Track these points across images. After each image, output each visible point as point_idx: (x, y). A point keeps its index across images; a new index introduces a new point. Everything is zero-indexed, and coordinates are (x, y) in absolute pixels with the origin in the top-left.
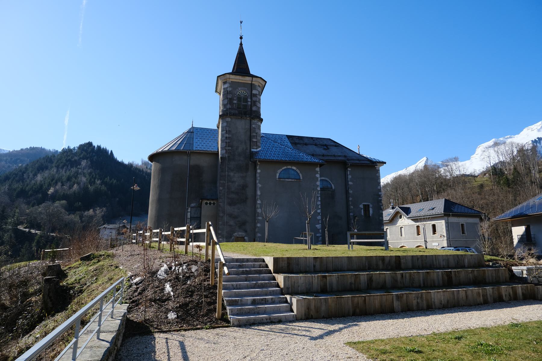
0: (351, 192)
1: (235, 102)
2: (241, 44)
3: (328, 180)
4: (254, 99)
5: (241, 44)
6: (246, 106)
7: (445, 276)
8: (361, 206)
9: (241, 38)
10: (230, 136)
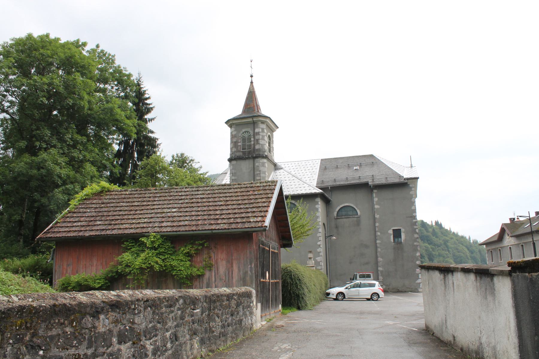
0: (377, 216)
1: (240, 144)
2: (252, 83)
3: (352, 205)
4: (257, 137)
5: (252, 83)
6: (250, 146)
7: (303, 305)
8: (391, 232)
9: (252, 76)
10: (236, 178)
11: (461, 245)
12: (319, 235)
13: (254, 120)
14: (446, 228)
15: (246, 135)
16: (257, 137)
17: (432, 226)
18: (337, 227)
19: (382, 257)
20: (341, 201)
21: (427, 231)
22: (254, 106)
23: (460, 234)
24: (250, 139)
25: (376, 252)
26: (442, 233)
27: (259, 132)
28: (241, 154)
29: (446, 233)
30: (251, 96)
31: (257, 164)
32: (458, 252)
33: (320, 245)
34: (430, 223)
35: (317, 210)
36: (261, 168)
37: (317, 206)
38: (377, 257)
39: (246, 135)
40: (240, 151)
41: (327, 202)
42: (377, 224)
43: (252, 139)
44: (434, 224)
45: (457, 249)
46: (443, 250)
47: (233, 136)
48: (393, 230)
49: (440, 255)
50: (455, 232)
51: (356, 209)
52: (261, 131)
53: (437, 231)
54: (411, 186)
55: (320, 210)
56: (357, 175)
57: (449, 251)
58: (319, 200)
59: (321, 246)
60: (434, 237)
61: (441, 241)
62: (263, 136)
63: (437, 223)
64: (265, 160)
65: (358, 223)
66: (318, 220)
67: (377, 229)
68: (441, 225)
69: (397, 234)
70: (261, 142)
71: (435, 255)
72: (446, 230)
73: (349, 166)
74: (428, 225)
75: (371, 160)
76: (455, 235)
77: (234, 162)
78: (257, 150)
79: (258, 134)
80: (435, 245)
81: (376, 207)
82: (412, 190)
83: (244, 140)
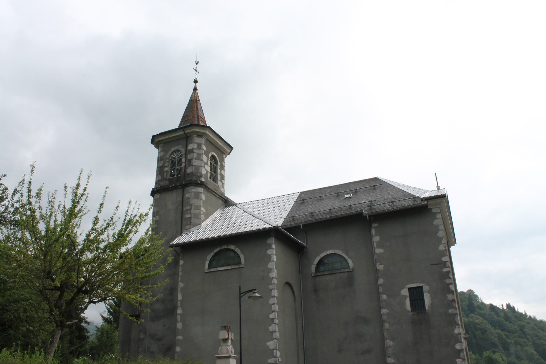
0: (380, 267)
1: (166, 169)
2: (195, 89)
3: (340, 252)
4: (189, 157)
5: (195, 89)
8: (405, 292)
9: (196, 82)
11: (541, 331)
12: (272, 301)
13: (186, 132)
14: (520, 311)
15: (176, 156)
16: (189, 157)
17: (503, 309)
18: (316, 291)
19: (392, 339)
20: (323, 248)
21: (498, 315)
22: (194, 117)
23: (538, 318)
24: (181, 160)
25: (382, 331)
26: (516, 317)
27: (193, 149)
28: (167, 182)
29: (522, 317)
30: (194, 105)
31: (187, 196)
32: (539, 339)
33: (273, 319)
34: (501, 307)
35: (269, 258)
36: (193, 201)
37: (269, 252)
38: (383, 339)
39: (176, 156)
40: (166, 179)
41: (298, 250)
42: (381, 281)
43: (183, 160)
44: (505, 308)
45: (537, 336)
46: (519, 337)
47: (160, 159)
48: (410, 289)
49: (517, 343)
50: (532, 316)
51: (346, 257)
52: (195, 146)
53: (510, 315)
54: (434, 211)
55: (274, 258)
56: (346, 204)
57: (527, 339)
58: (272, 241)
59: (276, 321)
60: (507, 323)
61: (515, 327)
62: (199, 155)
63: (508, 306)
64: (201, 190)
65: (350, 281)
66: (272, 275)
67: (381, 289)
68: (514, 308)
69: (416, 295)
70: (195, 163)
71: (511, 343)
72: (521, 314)
73: (338, 195)
74: (498, 308)
75: (375, 184)
76: (532, 320)
77: (157, 196)
78: (189, 174)
79: (192, 151)
80: (509, 331)
81: (378, 251)
82: (436, 219)
83: (173, 163)
